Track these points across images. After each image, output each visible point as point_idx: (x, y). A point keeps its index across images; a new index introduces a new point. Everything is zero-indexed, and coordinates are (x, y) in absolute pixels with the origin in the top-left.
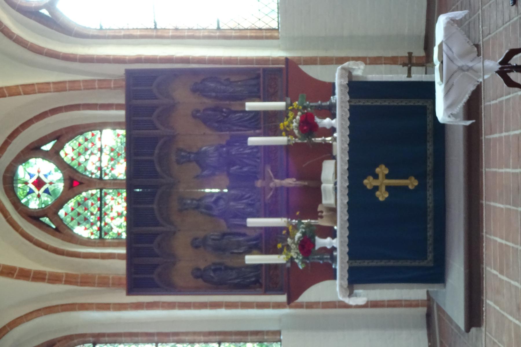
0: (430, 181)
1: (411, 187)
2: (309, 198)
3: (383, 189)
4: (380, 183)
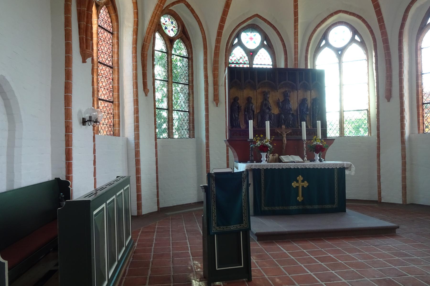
0: (301, 207)
1: (298, 198)
2: (279, 150)
3: (297, 185)
4: (300, 183)
